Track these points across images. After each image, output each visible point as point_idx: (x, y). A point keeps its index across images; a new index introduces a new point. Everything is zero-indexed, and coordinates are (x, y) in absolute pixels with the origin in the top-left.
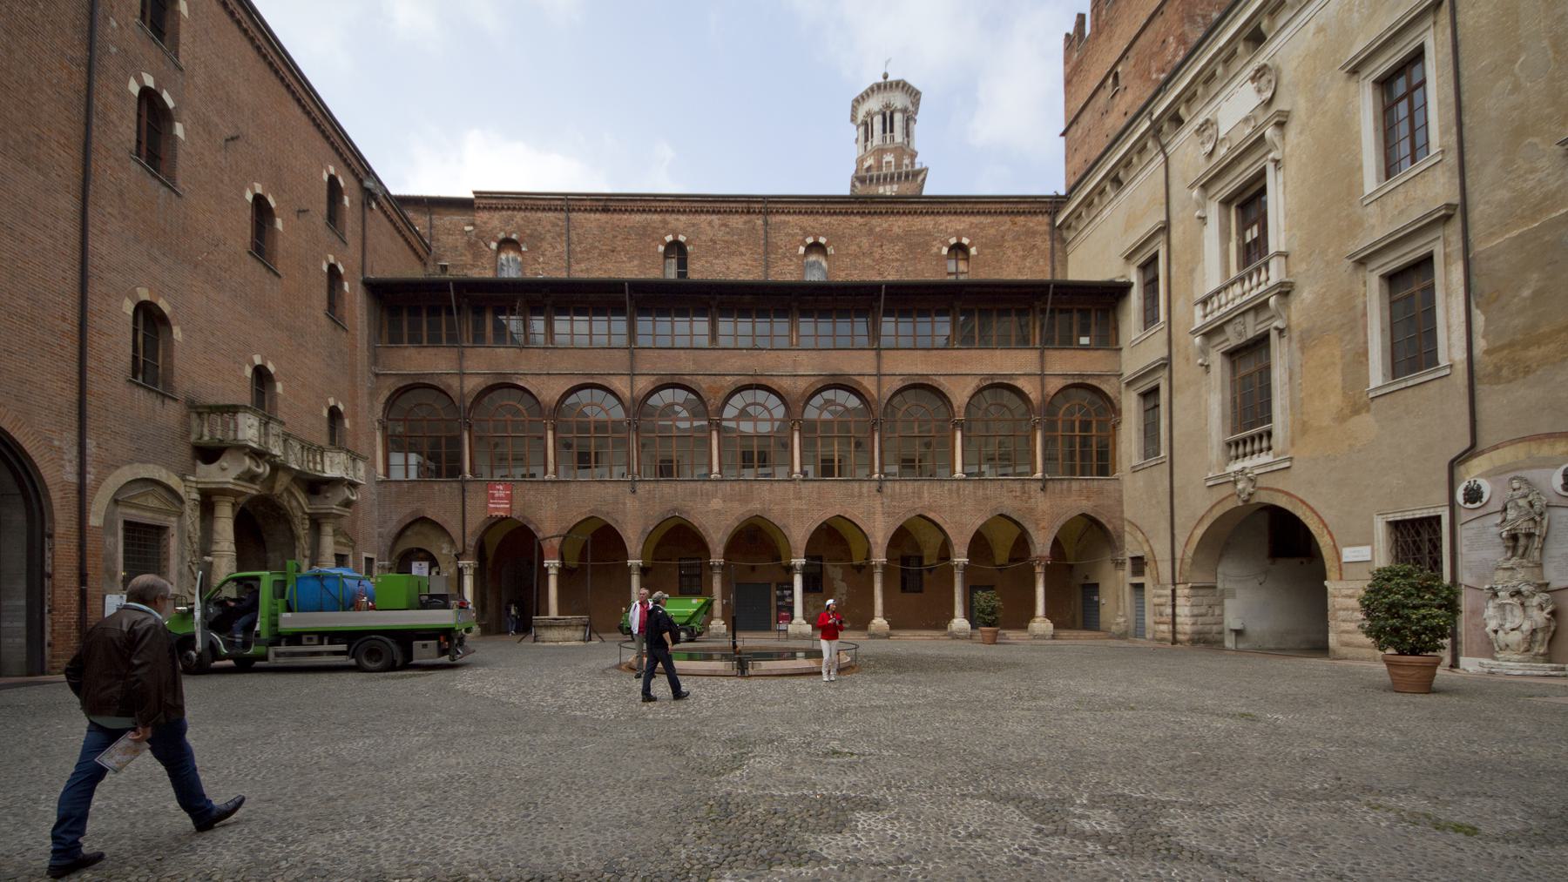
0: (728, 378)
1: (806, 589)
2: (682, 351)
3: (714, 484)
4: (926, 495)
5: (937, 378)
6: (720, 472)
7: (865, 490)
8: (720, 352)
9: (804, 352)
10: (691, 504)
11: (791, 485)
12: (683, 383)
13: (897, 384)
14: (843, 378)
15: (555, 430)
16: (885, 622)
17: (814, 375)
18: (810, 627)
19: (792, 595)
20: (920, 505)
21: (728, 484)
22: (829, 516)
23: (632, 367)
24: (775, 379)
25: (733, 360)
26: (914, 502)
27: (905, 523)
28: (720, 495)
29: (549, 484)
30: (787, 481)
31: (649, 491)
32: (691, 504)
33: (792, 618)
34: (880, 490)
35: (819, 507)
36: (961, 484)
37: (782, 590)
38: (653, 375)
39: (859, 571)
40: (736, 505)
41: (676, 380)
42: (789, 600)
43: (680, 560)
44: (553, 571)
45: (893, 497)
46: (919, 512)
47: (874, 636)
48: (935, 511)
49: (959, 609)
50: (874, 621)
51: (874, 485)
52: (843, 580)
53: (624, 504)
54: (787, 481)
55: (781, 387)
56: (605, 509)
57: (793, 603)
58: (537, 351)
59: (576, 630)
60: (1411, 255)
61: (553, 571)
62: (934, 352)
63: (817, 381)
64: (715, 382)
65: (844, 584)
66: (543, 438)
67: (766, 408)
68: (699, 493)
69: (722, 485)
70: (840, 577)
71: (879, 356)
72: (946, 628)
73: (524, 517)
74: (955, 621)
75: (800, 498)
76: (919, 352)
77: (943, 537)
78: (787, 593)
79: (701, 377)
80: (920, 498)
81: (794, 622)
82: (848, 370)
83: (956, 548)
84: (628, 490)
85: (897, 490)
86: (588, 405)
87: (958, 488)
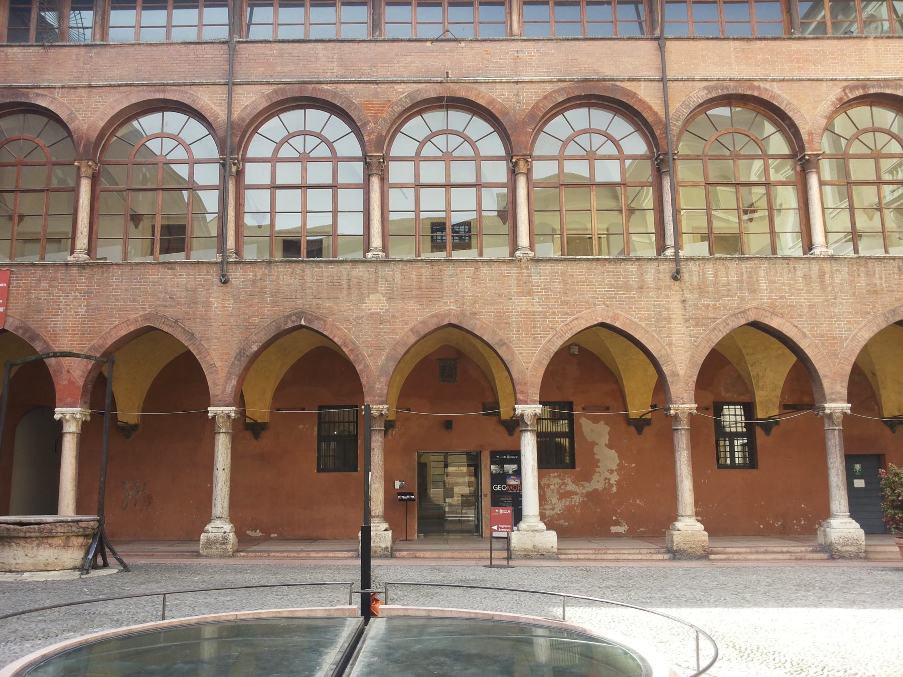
0: (399, 88)
1: (545, 461)
2: (320, 46)
3: (371, 268)
4: (763, 286)
5: (767, 85)
6: (384, 249)
7: (650, 277)
8: (387, 45)
9: (531, 45)
10: (328, 304)
11: (514, 270)
12: (320, 96)
13: (699, 94)
14: (601, 84)
15: (95, 179)
16: (700, 527)
17: (551, 82)
18: (553, 535)
19: (518, 473)
20: (755, 303)
21: (398, 268)
22: (584, 324)
23: (231, 72)
24: (483, 88)
25: (409, 59)
26: (742, 299)
27: (719, 344)
28: (382, 288)
29: (74, 270)
30: (370, 41)
31: (254, 281)
32: (328, 304)
33: (518, 517)
34: (676, 276)
35: (566, 309)
36: (827, 266)
37: (501, 463)
38: (268, 83)
39: (639, 430)
40: (412, 305)
41: (309, 91)
42: (512, 482)
43: (320, 408)
44: (71, 428)
45: (702, 290)
46: (752, 317)
47: (676, 554)
48: (782, 316)
49: (839, 501)
50: (678, 525)
51: (666, 269)
52: (610, 446)
53: (207, 305)
54: (370, 41)
55: (492, 101)
56: (170, 313)
57: (519, 487)
58: (75, 50)
59: (66, 546)
60: (430, 548)
61: (71, 428)
62: (759, 44)
63: (558, 91)
64: (376, 94)
65: (613, 453)
66: (75, 191)
67: (467, 139)
68: (344, 282)
69: (385, 270)
70: (605, 439)
71: (661, 49)
72: (814, 532)
73: (27, 329)
74: (834, 522)
75: (529, 293)
76: (732, 44)
77: (794, 359)
78: (510, 468)
79: (351, 86)
80: (753, 291)
81: (522, 525)
82: (608, 70)
83: (826, 383)
84: (216, 280)
85: (710, 277)
86: (155, 136)
87: (822, 275)
